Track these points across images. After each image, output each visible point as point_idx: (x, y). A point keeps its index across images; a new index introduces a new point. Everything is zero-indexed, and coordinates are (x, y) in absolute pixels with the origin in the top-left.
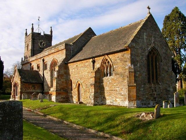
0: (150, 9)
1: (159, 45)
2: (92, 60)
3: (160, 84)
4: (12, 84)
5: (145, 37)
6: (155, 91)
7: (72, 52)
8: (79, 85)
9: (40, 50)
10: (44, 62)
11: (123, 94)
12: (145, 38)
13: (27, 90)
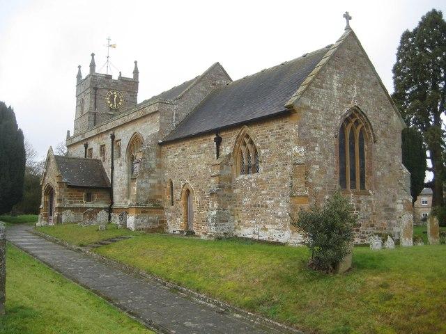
0: (350, 18)
1: (370, 102)
2: (214, 137)
3: (370, 195)
4: (43, 189)
5: (335, 85)
8: (188, 191)
9: (110, 113)
10: (116, 139)
11: (280, 213)
12: (335, 88)
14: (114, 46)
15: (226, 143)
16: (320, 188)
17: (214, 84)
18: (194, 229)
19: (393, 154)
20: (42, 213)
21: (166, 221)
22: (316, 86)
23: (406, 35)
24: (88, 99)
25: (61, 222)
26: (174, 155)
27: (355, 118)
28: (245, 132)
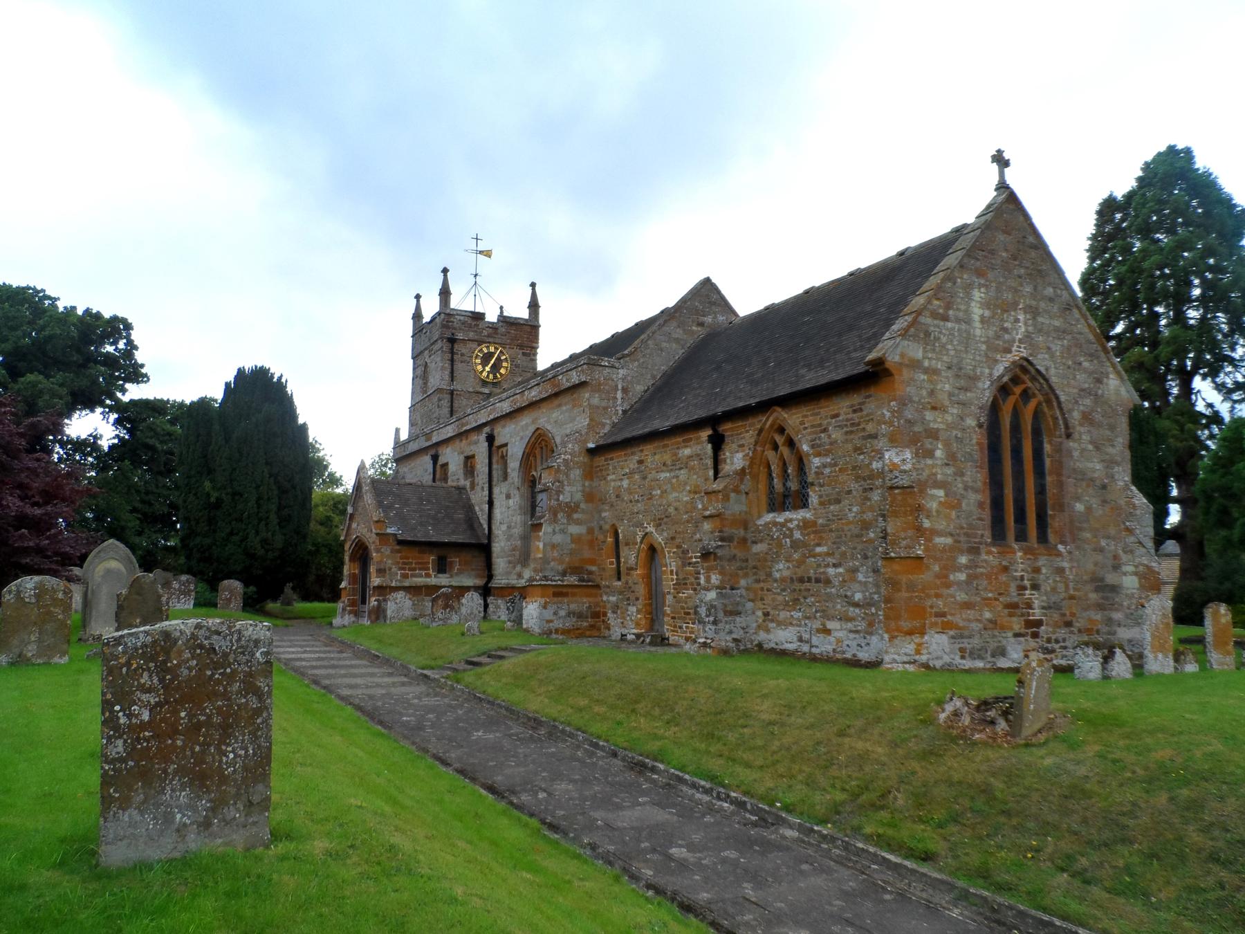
1: (1057, 347)
2: (705, 434)
3: (1059, 554)
4: (347, 547)
5: (977, 312)
6: (1035, 587)
7: (619, 395)
10: (497, 443)
11: (858, 597)
12: (976, 318)
13: (413, 576)
14: (488, 254)
15: (734, 446)
16: (949, 540)
17: (701, 324)
18: (667, 630)
19: (1110, 463)
20: (345, 599)
21: (605, 614)
22: (935, 315)
23: (1108, 208)
24: (438, 364)
25: (385, 617)
26: (621, 474)
27: (1022, 383)
28: (774, 422)
